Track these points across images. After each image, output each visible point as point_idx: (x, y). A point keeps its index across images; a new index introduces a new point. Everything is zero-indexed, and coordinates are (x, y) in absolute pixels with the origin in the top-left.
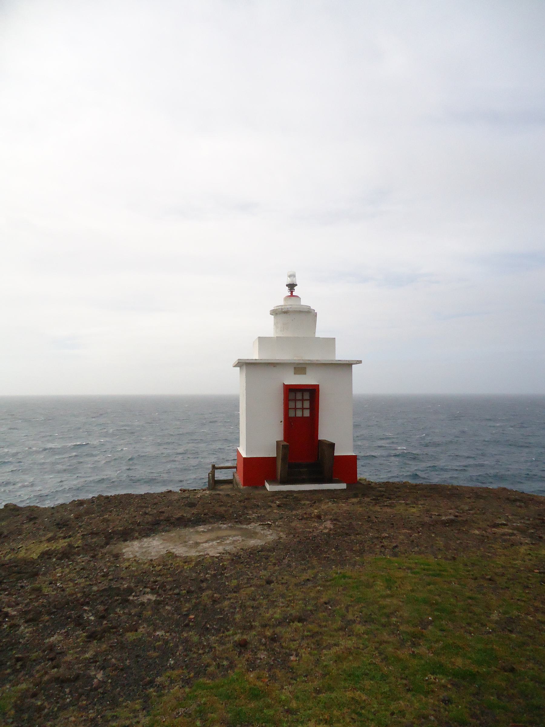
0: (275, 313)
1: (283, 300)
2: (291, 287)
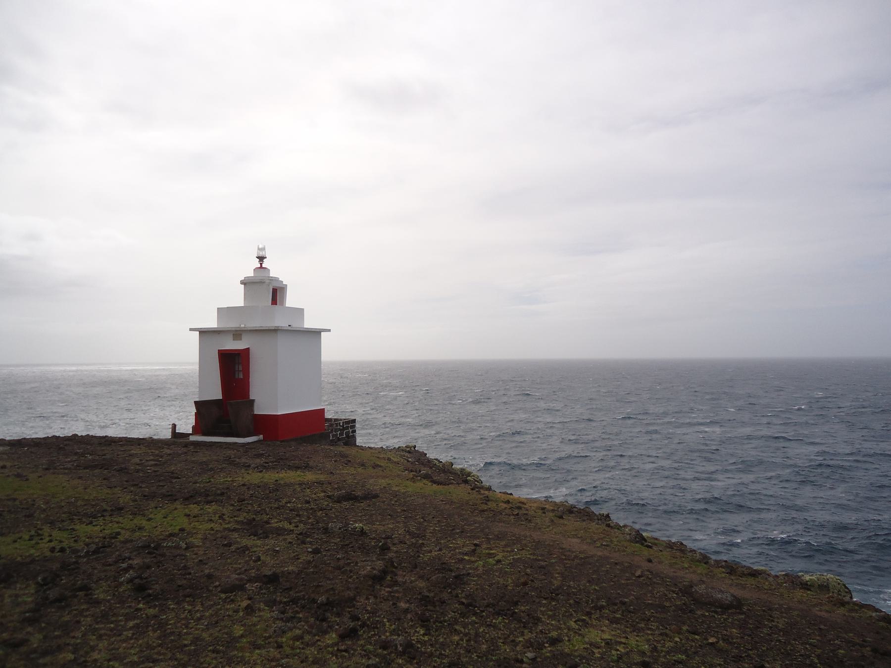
0: (245, 283)
1: (284, 279)
2: (261, 259)
